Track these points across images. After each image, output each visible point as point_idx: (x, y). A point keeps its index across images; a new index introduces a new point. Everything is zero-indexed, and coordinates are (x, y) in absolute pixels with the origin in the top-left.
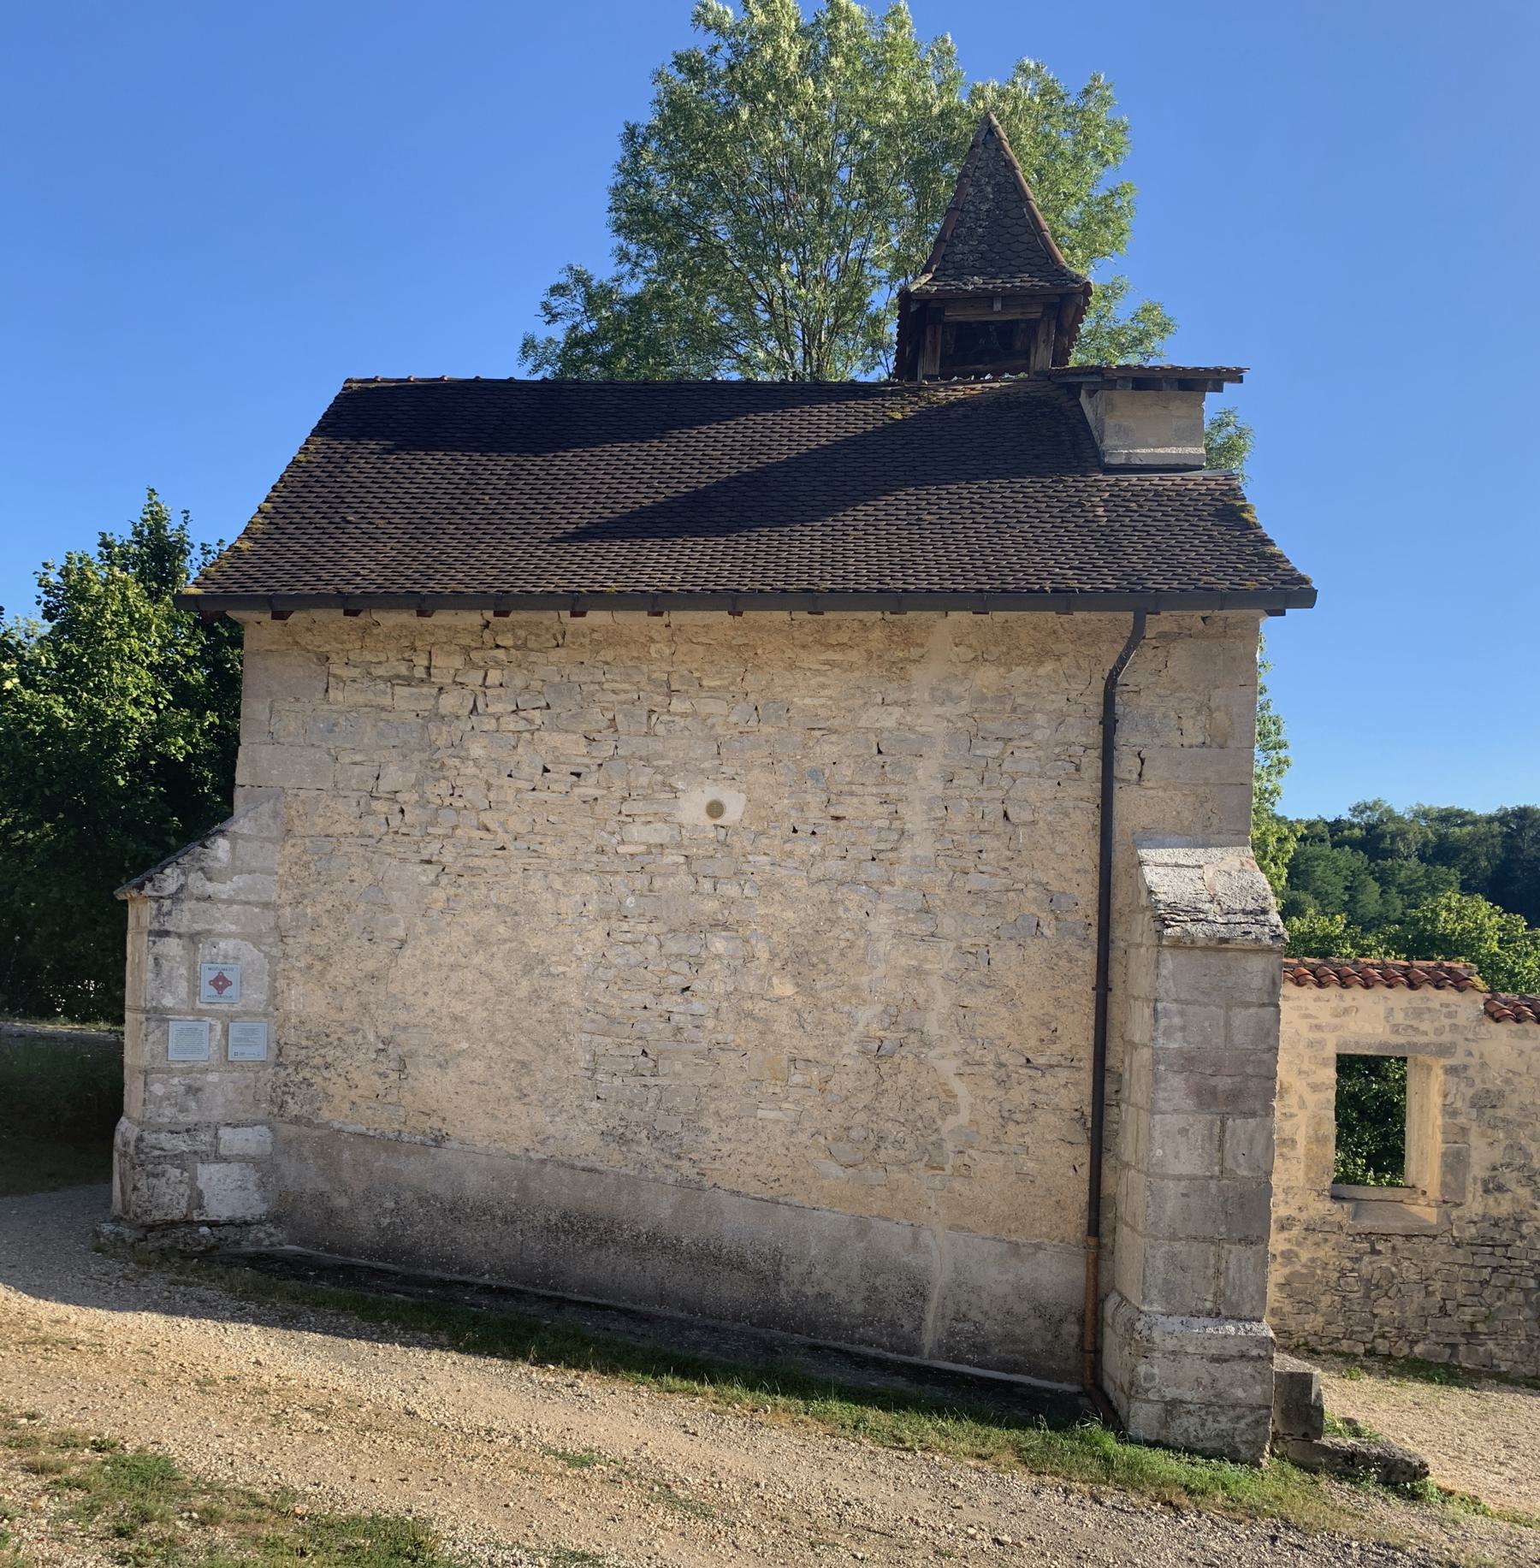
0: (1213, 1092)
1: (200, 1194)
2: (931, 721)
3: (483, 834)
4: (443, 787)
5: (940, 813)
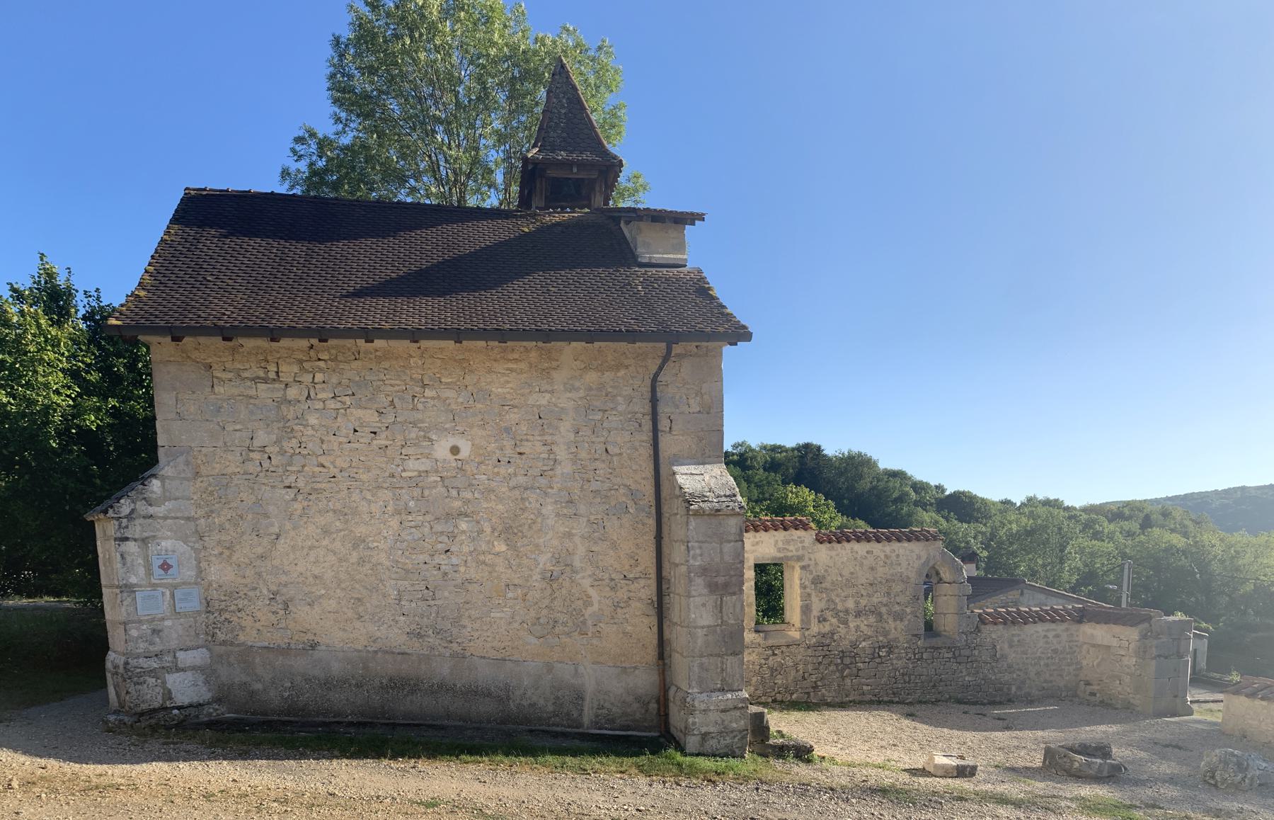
0: (716, 584)
1: (170, 692)
2: (565, 401)
3: (321, 469)
4: (294, 442)
5: (574, 450)
